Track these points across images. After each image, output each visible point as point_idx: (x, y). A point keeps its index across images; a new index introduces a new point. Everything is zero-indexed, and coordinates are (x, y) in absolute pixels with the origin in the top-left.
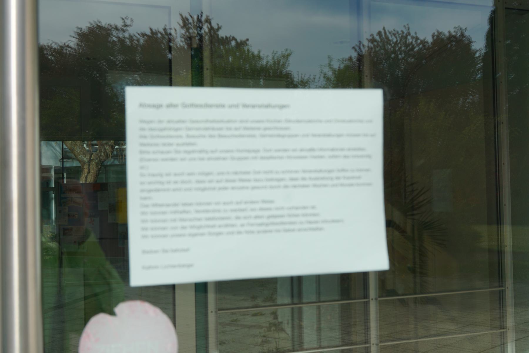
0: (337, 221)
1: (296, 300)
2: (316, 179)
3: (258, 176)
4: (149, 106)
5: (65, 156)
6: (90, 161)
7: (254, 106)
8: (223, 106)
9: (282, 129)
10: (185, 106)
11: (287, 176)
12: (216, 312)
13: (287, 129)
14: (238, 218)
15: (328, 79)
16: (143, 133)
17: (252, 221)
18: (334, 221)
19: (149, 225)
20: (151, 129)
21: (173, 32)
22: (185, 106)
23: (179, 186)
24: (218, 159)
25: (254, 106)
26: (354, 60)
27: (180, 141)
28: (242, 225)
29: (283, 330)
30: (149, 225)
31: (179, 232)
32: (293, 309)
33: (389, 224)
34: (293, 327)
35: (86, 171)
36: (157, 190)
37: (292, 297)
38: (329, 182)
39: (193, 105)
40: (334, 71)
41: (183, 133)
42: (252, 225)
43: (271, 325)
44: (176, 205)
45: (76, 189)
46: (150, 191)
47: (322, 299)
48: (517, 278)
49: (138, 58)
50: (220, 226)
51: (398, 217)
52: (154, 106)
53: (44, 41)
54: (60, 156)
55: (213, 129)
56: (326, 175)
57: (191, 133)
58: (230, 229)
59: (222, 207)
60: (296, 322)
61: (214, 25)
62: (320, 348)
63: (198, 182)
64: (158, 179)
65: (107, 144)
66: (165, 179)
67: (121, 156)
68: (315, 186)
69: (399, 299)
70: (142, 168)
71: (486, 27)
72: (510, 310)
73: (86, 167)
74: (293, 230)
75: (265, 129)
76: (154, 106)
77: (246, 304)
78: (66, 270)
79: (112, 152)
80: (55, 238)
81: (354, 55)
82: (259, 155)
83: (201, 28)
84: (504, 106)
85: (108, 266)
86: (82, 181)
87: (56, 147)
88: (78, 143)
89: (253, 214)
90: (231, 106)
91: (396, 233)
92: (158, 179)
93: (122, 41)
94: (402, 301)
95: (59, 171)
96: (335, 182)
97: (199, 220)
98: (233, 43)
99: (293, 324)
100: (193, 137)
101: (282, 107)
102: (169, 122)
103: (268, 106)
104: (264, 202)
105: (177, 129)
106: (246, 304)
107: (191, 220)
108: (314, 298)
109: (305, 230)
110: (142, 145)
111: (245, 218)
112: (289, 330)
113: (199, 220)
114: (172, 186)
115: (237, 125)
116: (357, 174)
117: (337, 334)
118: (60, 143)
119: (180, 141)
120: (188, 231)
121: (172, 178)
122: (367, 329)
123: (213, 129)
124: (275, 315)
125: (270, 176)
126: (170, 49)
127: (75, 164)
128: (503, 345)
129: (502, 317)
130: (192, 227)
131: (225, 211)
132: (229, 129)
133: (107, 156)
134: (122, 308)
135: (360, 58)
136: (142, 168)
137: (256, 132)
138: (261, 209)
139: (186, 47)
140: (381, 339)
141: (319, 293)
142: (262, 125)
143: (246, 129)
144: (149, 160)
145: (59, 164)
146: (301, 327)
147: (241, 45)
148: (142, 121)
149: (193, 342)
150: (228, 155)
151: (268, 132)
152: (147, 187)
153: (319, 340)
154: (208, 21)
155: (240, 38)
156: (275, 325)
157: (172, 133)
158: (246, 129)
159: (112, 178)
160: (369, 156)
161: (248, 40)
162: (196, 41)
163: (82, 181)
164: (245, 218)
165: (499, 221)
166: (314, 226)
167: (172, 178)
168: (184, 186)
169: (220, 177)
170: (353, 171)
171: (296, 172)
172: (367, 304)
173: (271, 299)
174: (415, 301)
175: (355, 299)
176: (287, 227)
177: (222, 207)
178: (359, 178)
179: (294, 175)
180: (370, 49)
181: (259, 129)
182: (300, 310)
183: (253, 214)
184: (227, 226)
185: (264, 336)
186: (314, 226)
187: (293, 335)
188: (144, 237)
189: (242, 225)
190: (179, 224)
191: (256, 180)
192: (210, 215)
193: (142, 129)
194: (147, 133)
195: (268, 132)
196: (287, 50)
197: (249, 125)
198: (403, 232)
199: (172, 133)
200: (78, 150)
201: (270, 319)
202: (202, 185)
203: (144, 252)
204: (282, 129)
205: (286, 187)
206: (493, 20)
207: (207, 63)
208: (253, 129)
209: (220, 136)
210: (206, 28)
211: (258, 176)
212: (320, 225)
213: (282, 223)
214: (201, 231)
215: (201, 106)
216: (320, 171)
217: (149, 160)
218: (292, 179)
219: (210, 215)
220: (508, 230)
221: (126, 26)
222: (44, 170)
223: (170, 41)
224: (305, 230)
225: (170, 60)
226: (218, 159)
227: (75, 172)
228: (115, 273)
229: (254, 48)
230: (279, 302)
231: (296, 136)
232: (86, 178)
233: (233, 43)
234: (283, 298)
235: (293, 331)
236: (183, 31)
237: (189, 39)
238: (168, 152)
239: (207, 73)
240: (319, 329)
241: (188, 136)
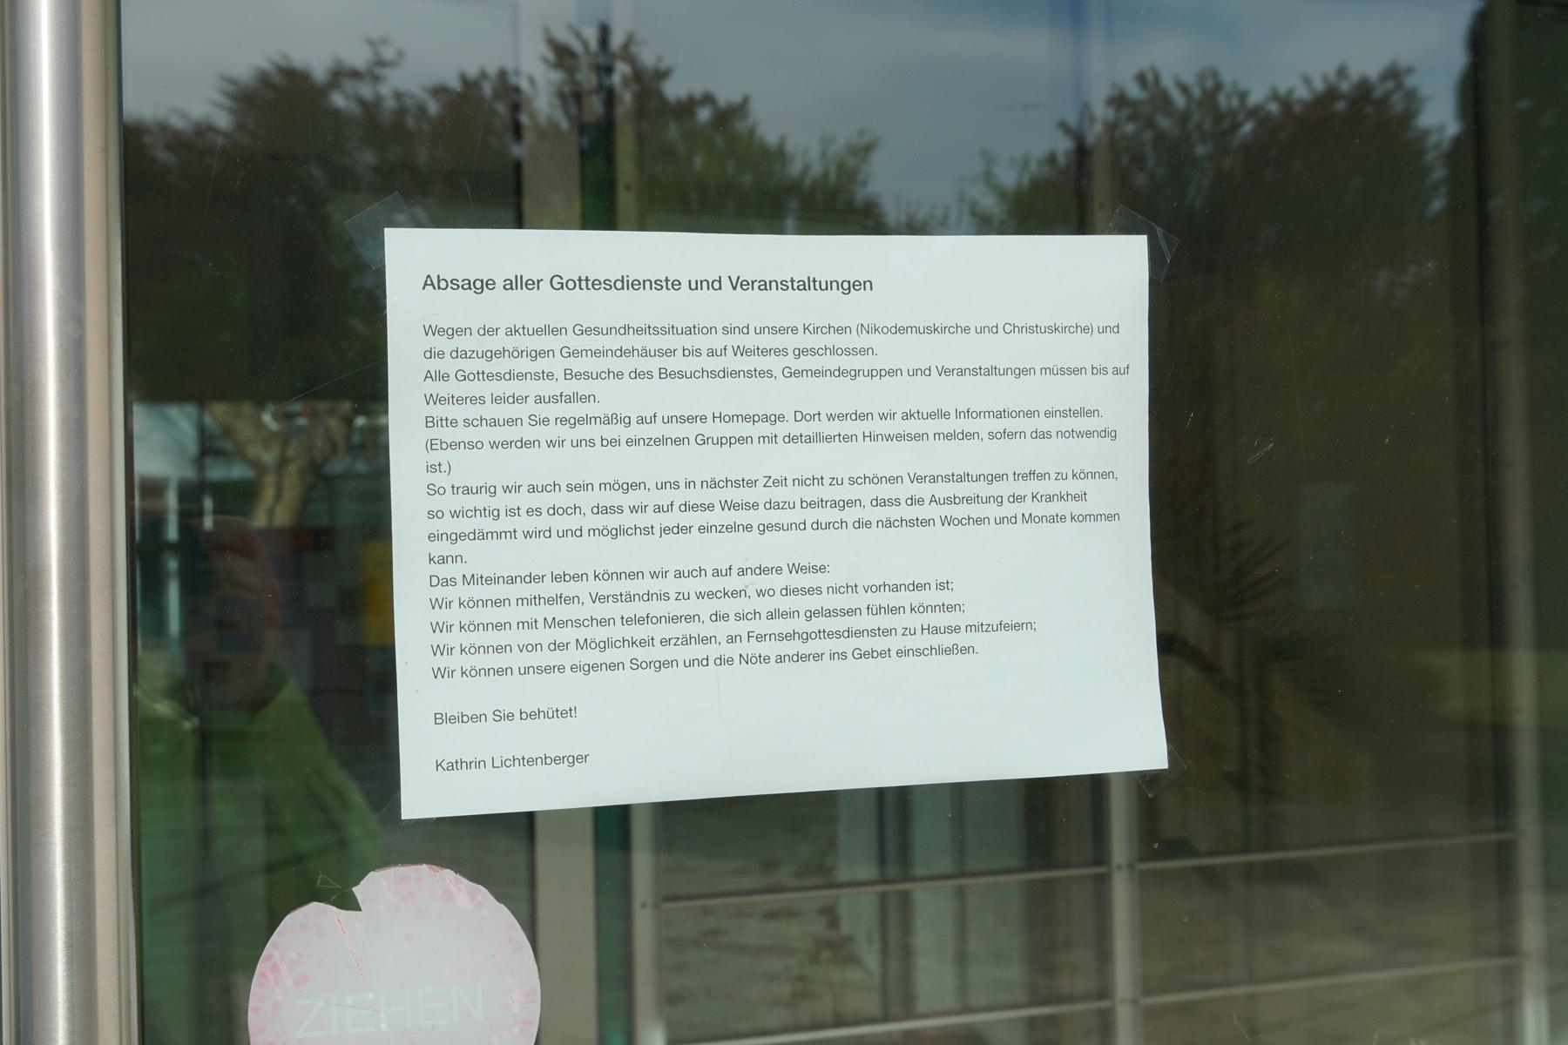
0: (1017, 627)
1: (893, 870)
2: (952, 500)
3: (778, 494)
4: (454, 284)
5: (208, 448)
6: (283, 462)
7: (765, 286)
8: (676, 285)
9: (848, 352)
10: (560, 284)
11: (866, 492)
12: (657, 906)
13: (864, 351)
14: (718, 617)
15: (989, 202)
16: (435, 365)
17: (762, 626)
18: (1002, 626)
19: (455, 638)
20: (459, 354)
21: (524, 85)
22: (560, 284)
23: (542, 522)
24: (662, 441)
25: (765, 286)
26: (1061, 159)
27: (546, 388)
28: (732, 639)
29: (853, 960)
30: (455, 638)
31: (545, 658)
32: (883, 897)
33: (1168, 644)
34: (884, 952)
35: (269, 493)
36: (481, 535)
37: (882, 860)
38: (991, 510)
39: (583, 283)
40: (1002, 194)
41: (556, 365)
42: (761, 638)
43: (821, 944)
44: (534, 579)
45: (243, 546)
46: (459, 537)
47: (972, 865)
48: (1551, 805)
49: (423, 156)
50: (665, 642)
51: (1194, 625)
52: (469, 285)
53: (142, 105)
54: (192, 447)
55: (645, 353)
56: (982, 489)
57: (578, 365)
58: (698, 651)
59: (670, 585)
60: (894, 934)
61: (647, 58)
62: (966, 1010)
63: (600, 510)
64: (482, 501)
65: (331, 412)
66: (502, 501)
67: (375, 446)
68: (947, 521)
69: (1200, 870)
70: (433, 468)
71: (1456, 59)
72: (1531, 902)
73: (270, 480)
74: (885, 653)
75: (800, 353)
76: (469, 285)
77: (746, 883)
78: (217, 785)
79: (348, 437)
80: (177, 691)
81: (1063, 145)
82: (781, 429)
83: (609, 70)
84: (1511, 293)
85: (337, 775)
86: (259, 520)
87: (183, 419)
88: (247, 408)
89: (765, 605)
90: (697, 286)
91: (1190, 672)
92: (482, 501)
93: (370, 108)
94: (1210, 876)
95: (191, 494)
96: (1009, 509)
97: (603, 622)
98: (704, 114)
99: (884, 942)
100: (587, 375)
101: (850, 287)
102: (512, 331)
103: (808, 284)
104: (797, 569)
105: (539, 354)
106: (746, 883)
107: (579, 623)
108: (945, 864)
109: (919, 652)
110: (432, 399)
111: (740, 617)
112: (872, 960)
113: (603, 622)
114: (523, 523)
115: (717, 341)
116: (1074, 487)
117: (1014, 972)
118: (191, 409)
119: (546, 388)
120: (572, 656)
121: (525, 500)
122: (1104, 956)
123: (645, 353)
124: (830, 914)
125: (813, 493)
126: (517, 130)
127: (238, 472)
128: (1511, 1005)
129: (1507, 921)
130: (583, 644)
131: (681, 596)
132: (689, 352)
133: (334, 447)
134: (375, 887)
135: (1082, 152)
136: (433, 468)
137: (774, 363)
138: (788, 591)
139: (564, 124)
140: (1147, 986)
141: (961, 851)
142: (789, 341)
143: (741, 351)
144: (454, 445)
145: (190, 473)
146: (907, 952)
147: (728, 116)
148: (431, 330)
149: (585, 997)
150: (690, 430)
151: (806, 362)
152: (448, 525)
153: (963, 990)
154: (627, 54)
155: (727, 95)
156: (830, 945)
157: (523, 365)
158: (741, 351)
159: (349, 513)
160: (1111, 434)
161: (746, 100)
162: (595, 106)
163: (259, 520)
164: (740, 617)
165: (1497, 637)
166: (947, 640)
167: (525, 500)
168: (560, 523)
169: (664, 497)
170: (1060, 476)
171: (892, 480)
172: (1103, 882)
173: (820, 871)
174: (1248, 871)
175: (1067, 866)
176: (866, 643)
177: (670, 585)
178: (1081, 497)
179: (885, 491)
180: (1112, 127)
181: (778, 352)
182: (906, 900)
183: (765, 605)
184: (687, 640)
185: (801, 979)
186: (947, 640)
187: (884, 975)
188: (438, 673)
189: (732, 639)
190: (546, 636)
191: (772, 505)
192: (639, 608)
193: (432, 354)
194: (448, 365)
195: (806, 362)
196: (861, 133)
197: (750, 341)
198: (1209, 667)
199: (523, 365)
200: (245, 430)
201: (818, 927)
202: (612, 521)
203: (440, 719)
204: (848, 352)
205: (861, 524)
206: (1479, 41)
207: (626, 168)
208: (765, 352)
209: (664, 374)
210: (622, 69)
211: (778, 494)
212: (962, 639)
213: (850, 633)
214: (611, 655)
215: (608, 285)
216: (964, 478)
217: (454, 445)
218: (879, 502)
219: (639, 608)
220: (1523, 662)
221: (381, 63)
222: (142, 492)
223: (516, 108)
224: (919, 652)
225: (518, 167)
226: (662, 441)
227: (238, 497)
228: (356, 795)
229: (768, 126)
230: (843, 874)
231: (891, 373)
232: (271, 513)
233: (704, 114)
234: (854, 861)
235: (884, 964)
236: (557, 76)
237: (572, 97)
238: (510, 422)
239: (626, 201)
240: (962, 959)
241: (569, 374)
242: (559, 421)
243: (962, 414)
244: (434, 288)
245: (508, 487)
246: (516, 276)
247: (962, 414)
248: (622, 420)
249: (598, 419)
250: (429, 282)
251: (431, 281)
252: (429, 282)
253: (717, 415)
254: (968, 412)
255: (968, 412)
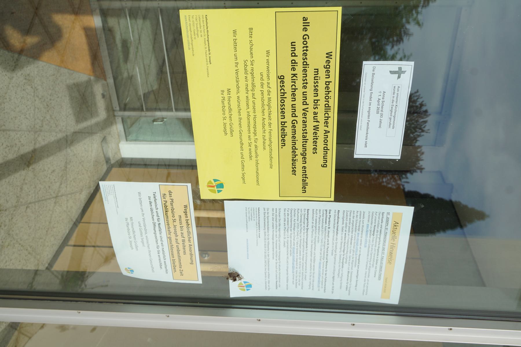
56: (275, 244)
242: (252, 69)
243: (248, 113)
244: (324, 134)
245: (392, 253)
246: (307, 183)
247: (248, 113)
248: (253, 89)
249: (253, 81)
250: (327, 132)
251: (327, 133)
252: (327, 132)
253: (256, 116)
254: (258, 163)
255: (258, 163)
